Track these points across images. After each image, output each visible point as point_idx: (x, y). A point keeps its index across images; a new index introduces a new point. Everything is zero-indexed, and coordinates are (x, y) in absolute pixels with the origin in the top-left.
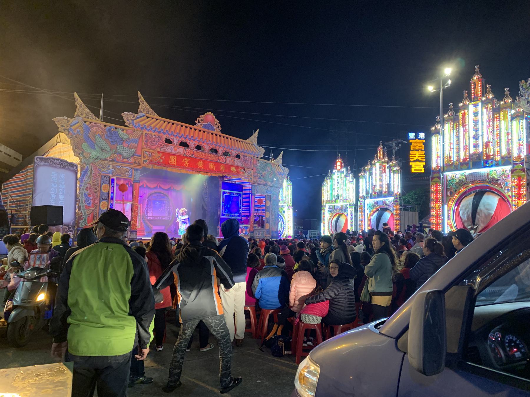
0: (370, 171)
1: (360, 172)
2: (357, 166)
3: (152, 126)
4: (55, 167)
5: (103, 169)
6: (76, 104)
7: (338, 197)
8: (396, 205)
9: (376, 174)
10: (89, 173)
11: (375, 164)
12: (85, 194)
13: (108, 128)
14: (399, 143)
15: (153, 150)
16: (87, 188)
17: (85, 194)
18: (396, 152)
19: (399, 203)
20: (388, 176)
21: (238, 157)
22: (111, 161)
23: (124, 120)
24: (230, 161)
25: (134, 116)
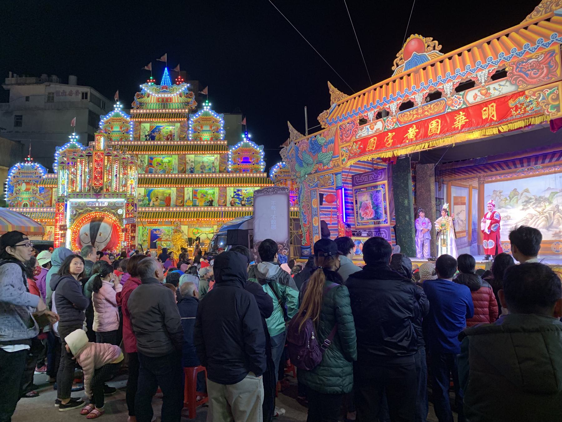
3: (354, 108)
4: (269, 195)
10: (303, 191)
22: (315, 173)
24: (475, 96)
25: (327, 113)
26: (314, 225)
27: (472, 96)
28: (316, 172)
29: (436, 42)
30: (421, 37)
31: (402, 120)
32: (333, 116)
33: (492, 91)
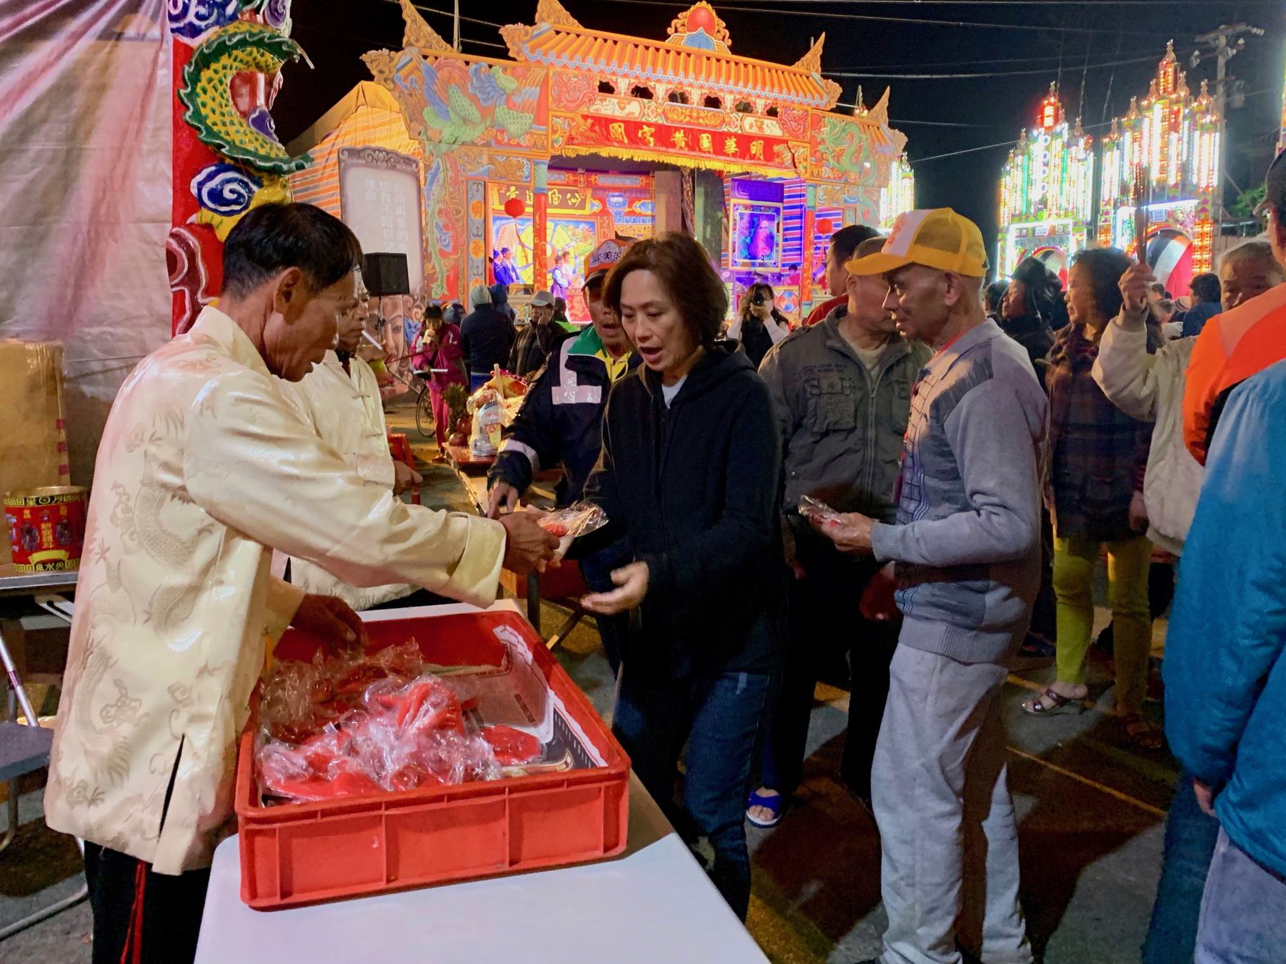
0: (1135, 127)
1: (1107, 130)
2: (1099, 111)
4: (377, 167)
5: (469, 167)
6: (404, 16)
7: (1044, 202)
8: (1203, 222)
9: (1151, 136)
11: (1149, 107)
12: (437, 225)
13: (473, 67)
14: (1238, 36)
15: (571, 111)
16: (440, 212)
17: (437, 225)
18: (1227, 63)
19: (1210, 215)
20: (1185, 139)
21: (772, 112)
23: (504, 44)
24: (751, 126)
26: (473, 256)
30: (714, 13)
31: (670, 116)
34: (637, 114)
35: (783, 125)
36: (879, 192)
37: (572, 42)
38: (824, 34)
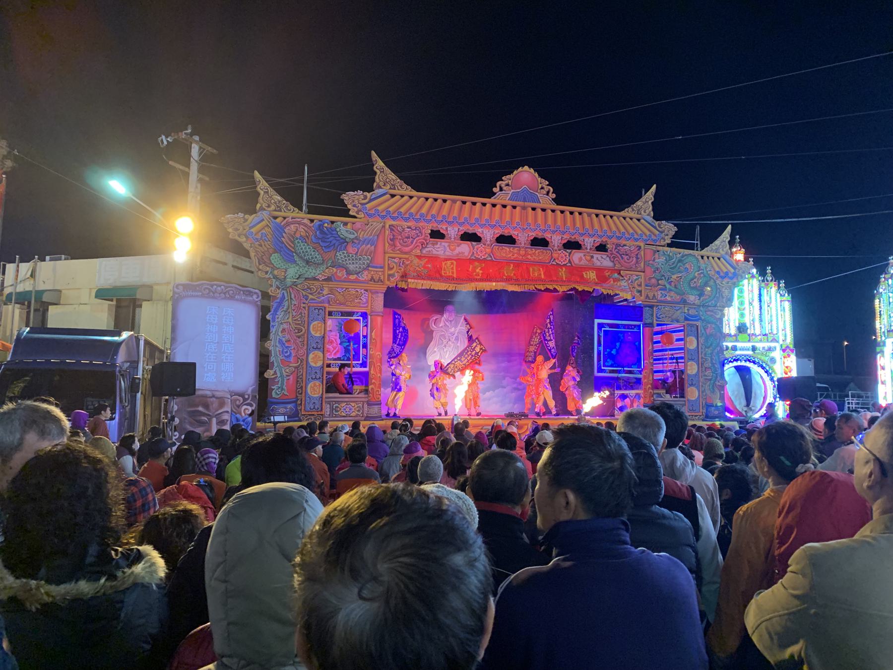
4: (214, 298)
15: (406, 253)
21: (602, 248)
24: (580, 259)
25: (365, 197)
27: (577, 257)
28: (328, 279)
29: (552, 190)
30: (536, 175)
32: (380, 205)
33: (595, 259)
34: (466, 254)
35: (613, 259)
36: (722, 311)
37: (441, 207)
38: (655, 186)
